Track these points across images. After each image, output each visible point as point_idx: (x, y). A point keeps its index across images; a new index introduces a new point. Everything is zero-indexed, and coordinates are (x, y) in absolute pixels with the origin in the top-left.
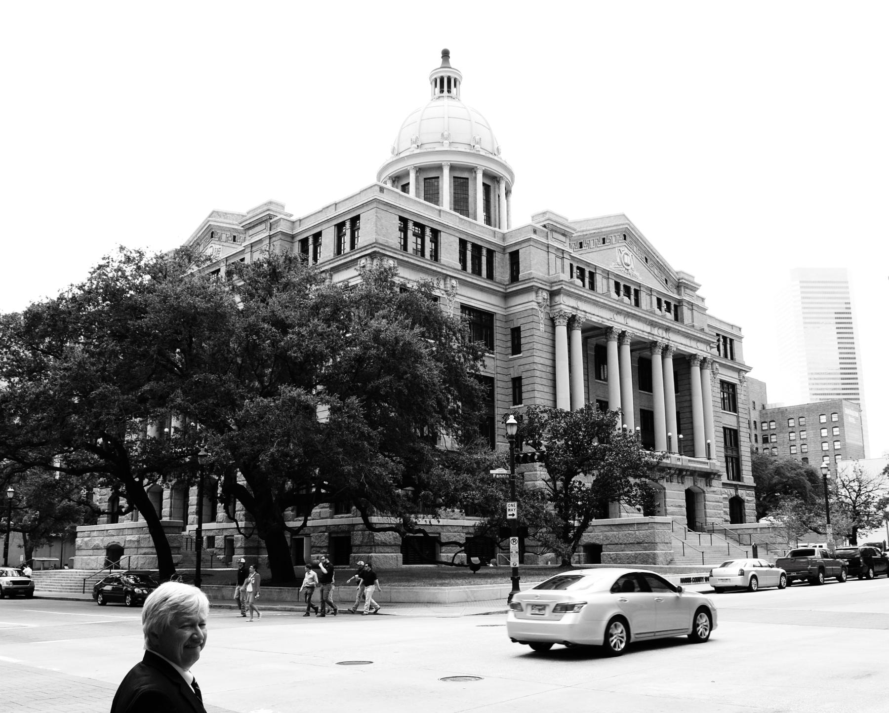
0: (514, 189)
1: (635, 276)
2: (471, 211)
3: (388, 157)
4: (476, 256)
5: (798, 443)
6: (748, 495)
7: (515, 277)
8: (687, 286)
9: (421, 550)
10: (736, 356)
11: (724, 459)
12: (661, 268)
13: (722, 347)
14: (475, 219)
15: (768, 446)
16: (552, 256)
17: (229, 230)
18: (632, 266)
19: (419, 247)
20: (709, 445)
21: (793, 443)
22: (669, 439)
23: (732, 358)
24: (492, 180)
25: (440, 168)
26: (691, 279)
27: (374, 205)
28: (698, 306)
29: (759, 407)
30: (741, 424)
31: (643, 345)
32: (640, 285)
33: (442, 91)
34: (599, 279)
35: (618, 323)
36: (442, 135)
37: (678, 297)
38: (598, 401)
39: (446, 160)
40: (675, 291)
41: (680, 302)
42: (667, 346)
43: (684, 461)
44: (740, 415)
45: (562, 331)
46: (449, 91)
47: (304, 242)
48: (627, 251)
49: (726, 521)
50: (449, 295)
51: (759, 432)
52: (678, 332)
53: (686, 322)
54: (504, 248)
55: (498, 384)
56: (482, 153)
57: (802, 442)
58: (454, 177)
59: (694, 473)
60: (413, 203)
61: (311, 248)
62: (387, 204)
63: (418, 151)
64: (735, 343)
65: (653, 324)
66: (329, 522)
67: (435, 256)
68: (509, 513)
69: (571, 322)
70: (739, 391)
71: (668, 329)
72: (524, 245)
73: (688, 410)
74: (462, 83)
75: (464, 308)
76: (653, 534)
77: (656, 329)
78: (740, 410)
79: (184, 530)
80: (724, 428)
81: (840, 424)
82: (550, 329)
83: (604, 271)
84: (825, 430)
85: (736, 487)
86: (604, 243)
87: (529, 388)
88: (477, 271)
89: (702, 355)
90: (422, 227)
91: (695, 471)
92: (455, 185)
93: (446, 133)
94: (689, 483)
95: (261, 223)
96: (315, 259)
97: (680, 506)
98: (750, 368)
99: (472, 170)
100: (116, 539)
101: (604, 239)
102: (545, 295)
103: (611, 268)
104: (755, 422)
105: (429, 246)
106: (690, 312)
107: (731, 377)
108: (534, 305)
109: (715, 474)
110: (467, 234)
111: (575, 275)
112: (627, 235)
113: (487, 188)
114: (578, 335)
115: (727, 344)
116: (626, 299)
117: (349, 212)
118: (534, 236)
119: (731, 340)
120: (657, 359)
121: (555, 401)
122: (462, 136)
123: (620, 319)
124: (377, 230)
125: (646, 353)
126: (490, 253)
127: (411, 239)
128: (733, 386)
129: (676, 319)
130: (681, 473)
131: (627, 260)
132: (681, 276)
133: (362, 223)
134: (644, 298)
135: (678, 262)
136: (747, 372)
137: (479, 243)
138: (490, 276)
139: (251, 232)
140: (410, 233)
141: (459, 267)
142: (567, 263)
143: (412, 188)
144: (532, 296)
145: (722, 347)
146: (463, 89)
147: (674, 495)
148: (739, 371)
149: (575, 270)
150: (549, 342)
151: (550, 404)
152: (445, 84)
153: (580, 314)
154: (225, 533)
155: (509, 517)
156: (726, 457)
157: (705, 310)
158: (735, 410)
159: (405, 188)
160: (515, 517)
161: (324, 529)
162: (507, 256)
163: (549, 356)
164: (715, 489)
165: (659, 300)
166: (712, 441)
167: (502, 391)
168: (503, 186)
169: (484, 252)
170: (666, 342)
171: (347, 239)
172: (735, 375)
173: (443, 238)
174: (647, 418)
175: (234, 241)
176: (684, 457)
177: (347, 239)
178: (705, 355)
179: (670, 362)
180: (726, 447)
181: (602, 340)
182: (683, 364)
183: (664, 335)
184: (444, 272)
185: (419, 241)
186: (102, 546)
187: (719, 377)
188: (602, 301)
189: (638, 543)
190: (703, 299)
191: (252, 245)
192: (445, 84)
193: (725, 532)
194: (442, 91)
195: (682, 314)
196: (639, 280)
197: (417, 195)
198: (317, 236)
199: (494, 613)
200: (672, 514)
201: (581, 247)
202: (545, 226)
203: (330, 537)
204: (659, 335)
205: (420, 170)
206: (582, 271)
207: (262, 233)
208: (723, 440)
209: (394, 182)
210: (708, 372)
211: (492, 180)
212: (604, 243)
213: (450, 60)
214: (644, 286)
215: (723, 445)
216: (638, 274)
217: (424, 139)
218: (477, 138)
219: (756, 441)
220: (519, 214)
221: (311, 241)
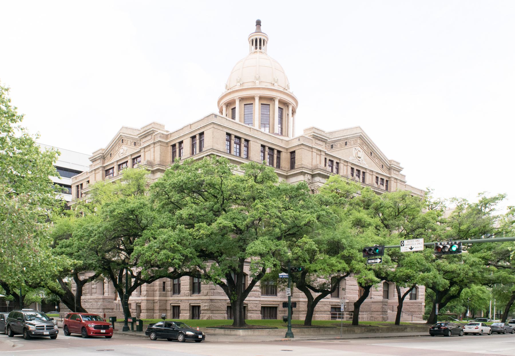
0: (298, 110)
17: (132, 138)
18: (362, 158)
27: (212, 126)
28: (401, 181)
33: (256, 48)
34: (341, 166)
36: (255, 77)
41: (389, 178)
46: (260, 48)
48: (360, 149)
54: (287, 149)
58: (262, 104)
60: (238, 126)
61: (177, 150)
74: (268, 42)
83: (345, 161)
90: (239, 138)
96: (180, 156)
99: (272, 99)
103: (350, 159)
105: (243, 149)
111: (327, 165)
116: (357, 178)
124: (215, 141)
126: (279, 152)
127: (234, 145)
129: (387, 189)
131: (360, 154)
134: (368, 177)
137: (273, 147)
139: (144, 140)
140: (233, 142)
146: (269, 46)
149: (328, 161)
152: (258, 43)
162: (289, 154)
169: (276, 152)
173: (251, 143)
175: (135, 145)
185: (238, 146)
192: (258, 43)
194: (256, 48)
198: (181, 143)
199: (103, 350)
201: (332, 148)
203: (190, 306)
205: (242, 99)
216: (365, 163)
218: (276, 79)
220: (299, 126)
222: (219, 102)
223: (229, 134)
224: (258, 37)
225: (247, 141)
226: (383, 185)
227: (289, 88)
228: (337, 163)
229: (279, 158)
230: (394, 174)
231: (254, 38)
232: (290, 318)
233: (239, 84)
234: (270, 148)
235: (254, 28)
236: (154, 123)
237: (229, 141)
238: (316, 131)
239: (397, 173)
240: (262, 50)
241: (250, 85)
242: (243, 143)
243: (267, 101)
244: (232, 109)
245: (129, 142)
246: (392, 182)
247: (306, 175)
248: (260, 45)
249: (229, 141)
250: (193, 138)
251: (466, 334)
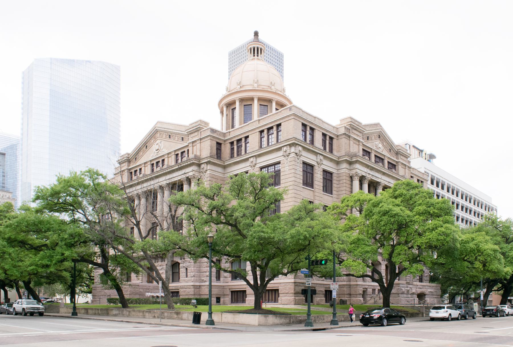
16: (351, 142)
17: (179, 134)
25: (252, 99)
33: (254, 56)
36: (254, 81)
37: (397, 160)
39: (256, 95)
40: (395, 156)
46: (258, 56)
99: (270, 101)
100: (423, 290)
105: (308, 137)
117: (275, 121)
132: (399, 148)
139: (192, 135)
141: (322, 148)
154: (364, 287)
171: (265, 140)
177: (265, 140)
191: (193, 142)
194: (254, 56)
205: (242, 100)
217: (243, 83)
222: (219, 105)
224: (256, 46)
230: (401, 160)
231: (252, 46)
232: (261, 311)
236: (200, 121)
240: (259, 57)
241: (250, 88)
244: (232, 109)
246: (400, 167)
248: (258, 53)
250: (262, 132)
251: (433, 319)
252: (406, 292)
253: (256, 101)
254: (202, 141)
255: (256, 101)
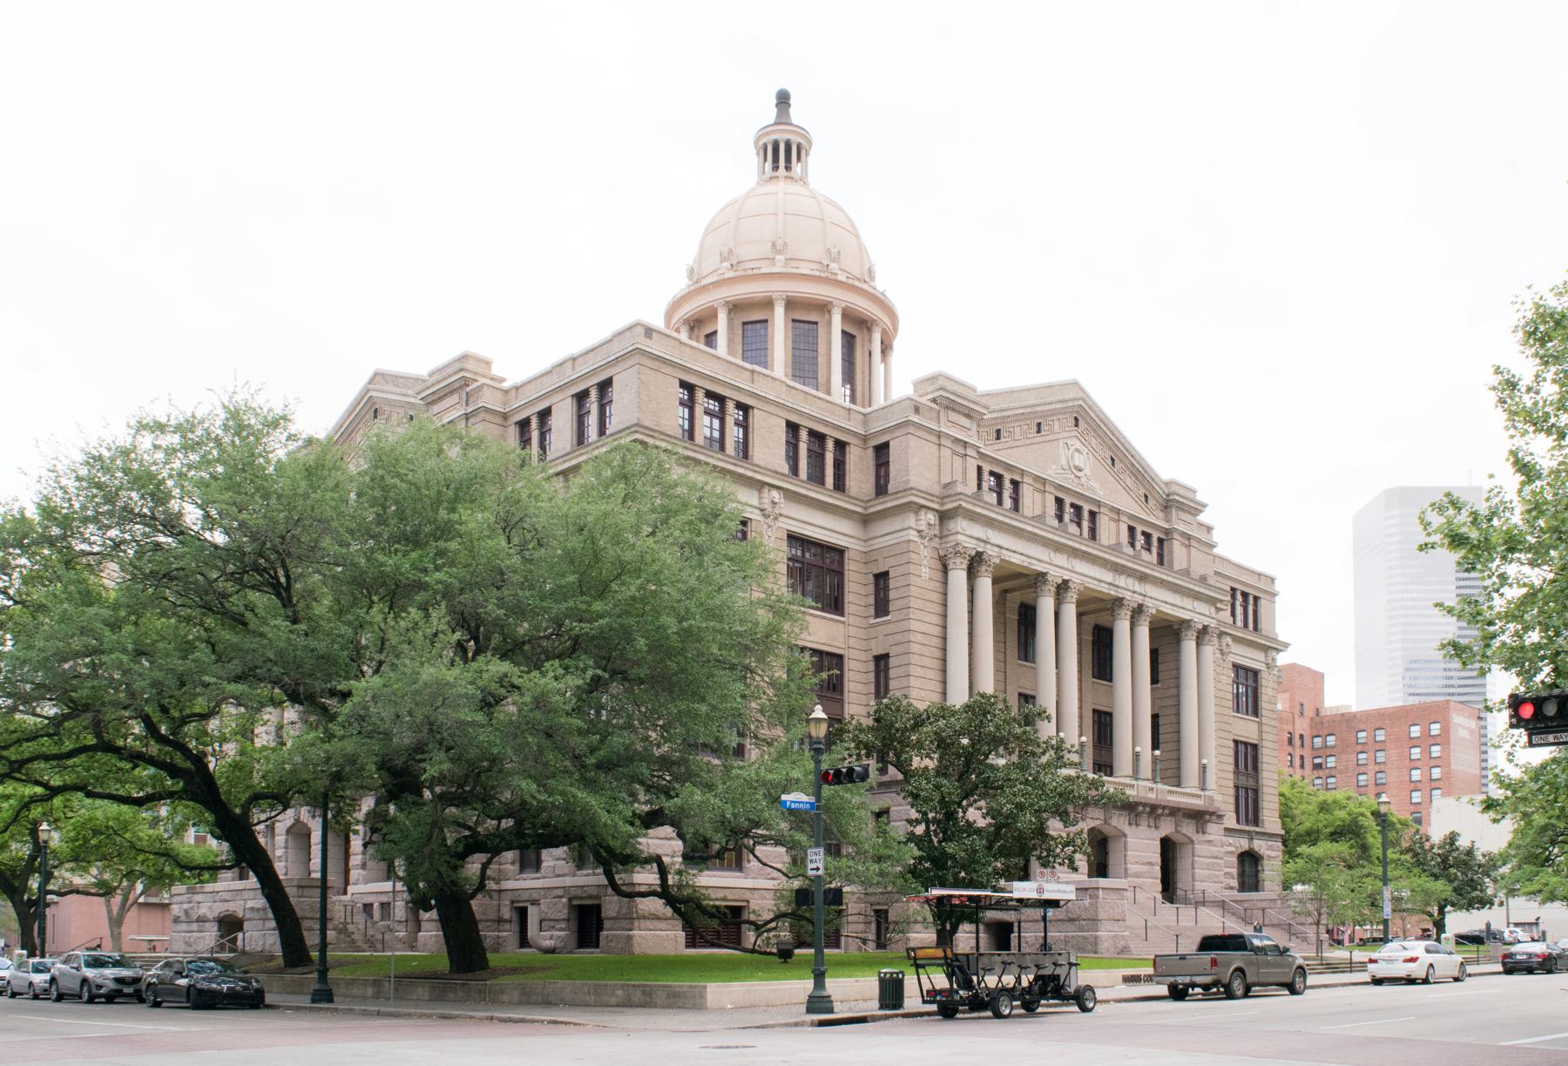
1: (1092, 489)
2: (822, 379)
3: (681, 284)
4: (817, 451)
5: (1372, 768)
6: (1270, 848)
7: (881, 489)
8: (1182, 507)
9: (715, 927)
10: (1263, 625)
11: (1232, 792)
12: (1139, 473)
13: (1239, 610)
14: (829, 393)
15: (1321, 773)
16: (946, 453)
18: (1087, 471)
19: (716, 434)
20: (1204, 767)
21: (1362, 769)
22: (1136, 756)
23: (1256, 628)
24: (858, 326)
25: (768, 304)
26: (1189, 494)
28: (1199, 541)
29: (1309, 713)
30: (1265, 736)
31: (1022, 581)
32: (1099, 504)
33: (776, 168)
34: (1027, 492)
35: (1056, 566)
36: (774, 244)
38: (1095, 711)
40: (1161, 515)
41: (1168, 532)
42: (1140, 606)
43: (1161, 793)
44: (1264, 720)
45: (958, 577)
46: (788, 168)
47: (524, 425)
48: (1078, 445)
49: (1231, 888)
50: (766, 516)
51: (1307, 753)
52: (1162, 583)
53: (1177, 567)
54: (865, 439)
55: (849, 665)
56: (842, 278)
57: (1377, 768)
59: (1174, 811)
60: (721, 363)
61: (535, 435)
62: (657, 358)
63: (731, 274)
64: (1263, 603)
65: (1117, 569)
66: (568, 881)
67: (744, 450)
68: (811, 866)
69: (975, 563)
70: (1264, 682)
71: (1143, 578)
72: (898, 433)
73: (1173, 711)
74: (811, 153)
75: (793, 538)
76: (1095, 906)
77: (1123, 578)
78: (1264, 712)
79: (345, 893)
80: (1236, 742)
81: (1444, 739)
82: (938, 576)
83: (1037, 478)
84: (1418, 750)
85: (1250, 836)
86: (1039, 431)
87: (901, 671)
88: (817, 477)
89: (1199, 621)
90: (721, 400)
91: (1179, 809)
92: (795, 335)
93: (779, 243)
94: (1167, 828)
95: (451, 393)
96: (543, 447)
97: (1150, 864)
98: (1286, 645)
99: (824, 307)
101: (1039, 425)
102: (932, 518)
103: (1051, 473)
104: (1301, 736)
105: (734, 433)
106: (1184, 550)
107: (1252, 659)
108: (913, 535)
109: (1212, 814)
110: (801, 413)
111: (985, 486)
112: (1082, 417)
113: (849, 340)
114: (985, 586)
115: (1248, 601)
116: (1073, 528)
118: (915, 419)
119: (1256, 599)
120: (1122, 628)
121: (944, 693)
122: (809, 252)
123: (1061, 559)
125: (1103, 620)
126: (841, 446)
128: (1256, 673)
129: (1161, 562)
130: (1154, 811)
131: (1079, 460)
132: (1174, 488)
133: (616, 392)
134: (1105, 526)
135: (1167, 463)
136: (1278, 651)
138: (840, 486)
139: (436, 408)
140: (699, 410)
141: (785, 469)
142: (972, 464)
143: (722, 339)
144: (910, 520)
145: (1239, 610)
146: (816, 164)
147: (1139, 848)
148: (1266, 649)
149: (986, 476)
150: (937, 597)
151: (936, 698)
152: (783, 153)
153: (991, 551)
155: (810, 873)
156: (1237, 787)
157: (1212, 546)
158: (1256, 713)
159: (710, 339)
160: (821, 872)
161: (560, 892)
162: (871, 452)
163: (937, 620)
164: (1211, 837)
165: (1131, 530)
166: (1211, 761)
167: (858, 677)
168: (877, 337)
169: (830, 445)
170: (1139, 599)
171: (592, 420)
172: (1260, 656)
173: (757, 418)
174: (1103, 725)
176: (1160, 786)
177: (592, 420)
178: (1206, 621)
179: (1144, 632)
180: (1237, 772)
181: (1025, 596)
182: (1167, 635)
183: (1137, 588)
184: (759, 477)
185: (716, 423)
186: (210, 917)
187: (1232, 658)
188: (1029, 528)
189: (1071, 920)
190: (1209, 529)
192: (783, 153)
193: (1222, 905)
194: (776, 168)
195: (1171, 552)
196: (1100, 495)
197: (731, 351)
198: (545, 415)
199: (772, 1026)
200: (1136, 875)
201: (998, 438)
202: (934, 400)
203: (571, 907)
204: (1127, 588)
205: (735, 307)
206: (1077, 509)
207: (452, 410)
208: (1232, 760)
209: (692, 329)
210: (1209, 651)
211: (858, 326)
212: (1039, 431)
213: (791, 110)
214: (1106, 505)
215: (1231, 768)
216: (1097, 486)
219: (1302, 766)
220: (899, 378)
221: (534, 423)
223: (688, 387)
225: (744, 408)
226: (1149, 550)
227: (872, 279)
228: (1015, 484)
229: (840, 465)
230: (1179, 523)
233: (727, 264)
234: (813, 433)
235: (771, 114)
237: (690, 404)
238: (949, 386)
239: (1187, 517)
242: (733, 414)
243: (806, 316)
245: (395, 417)
247: (922, 512)
249: (690, 404)
250: (581, 397)
252: (183, 918)
253: (779, 310)
254: (472, 420)
255: (779, 310)
